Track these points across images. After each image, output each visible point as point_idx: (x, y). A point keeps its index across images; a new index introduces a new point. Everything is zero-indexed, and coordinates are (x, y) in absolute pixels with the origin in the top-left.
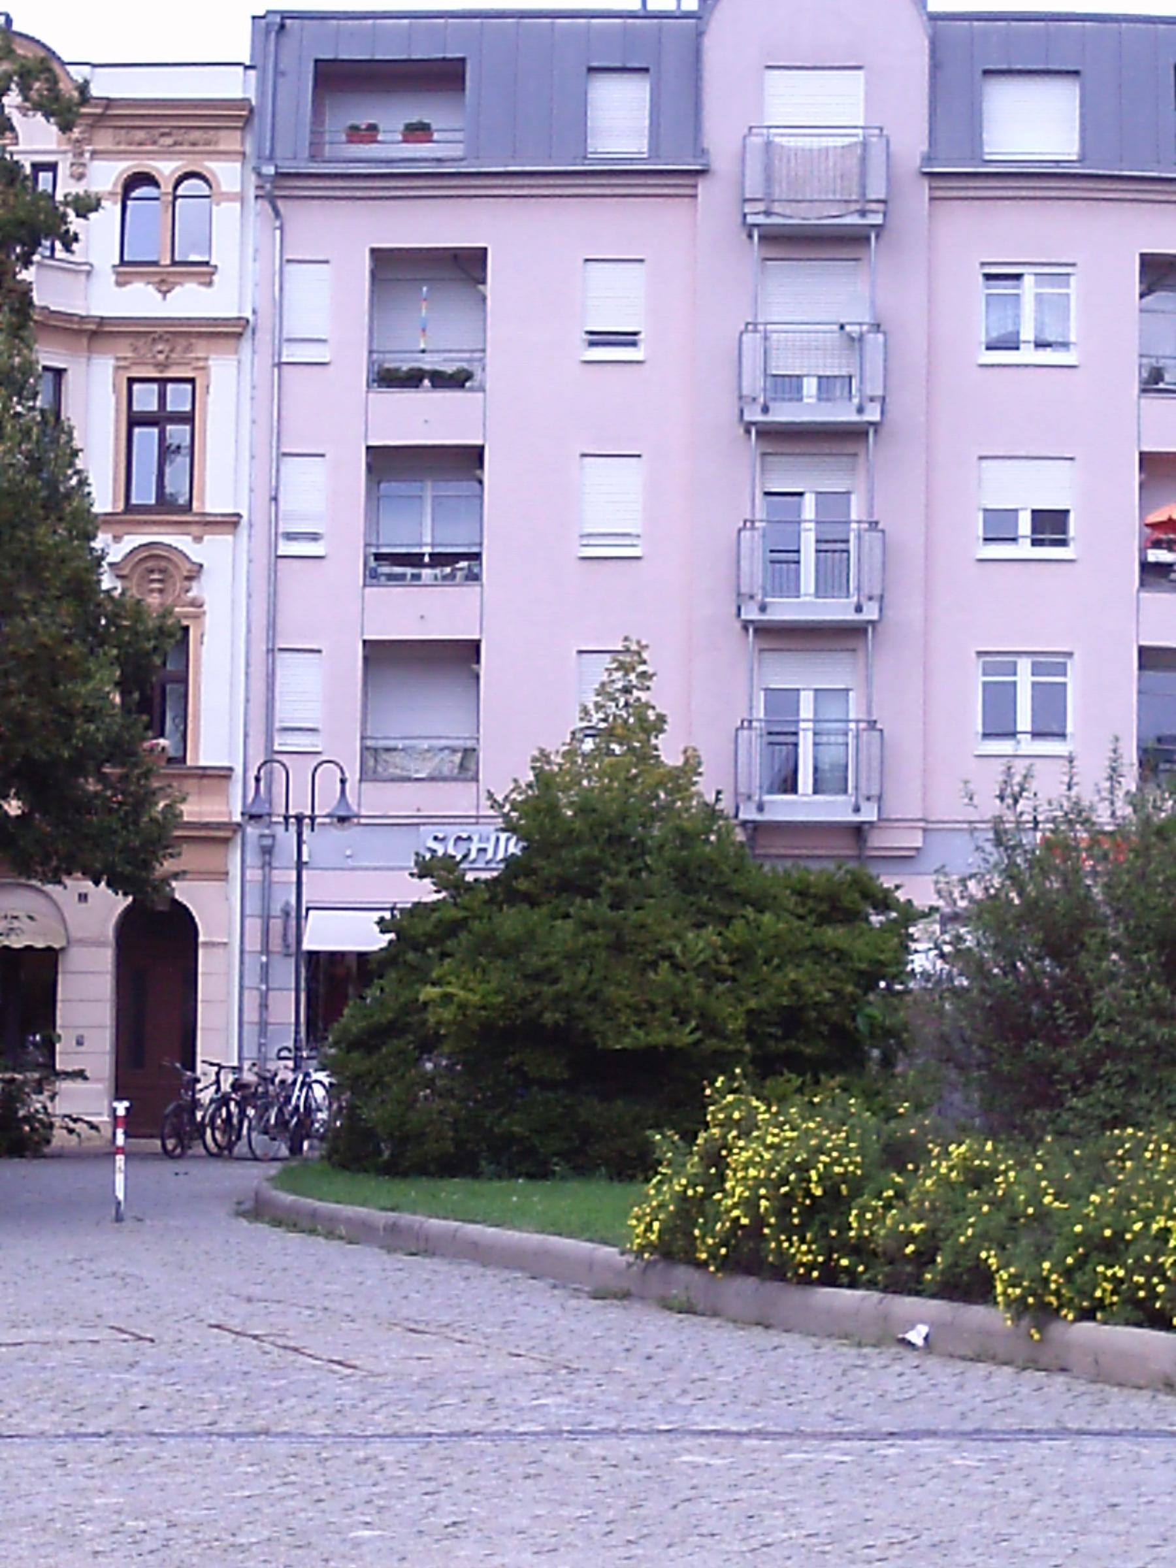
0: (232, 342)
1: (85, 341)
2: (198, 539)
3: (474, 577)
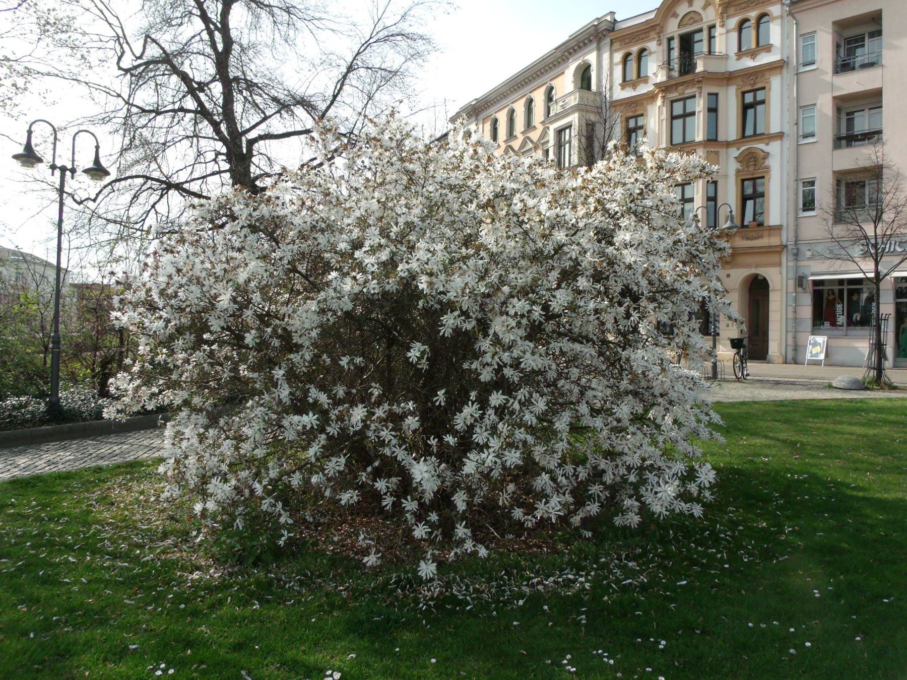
0: (779, 70)
1: (725, 82)
2: (767, 144)
3: (879, 140)
